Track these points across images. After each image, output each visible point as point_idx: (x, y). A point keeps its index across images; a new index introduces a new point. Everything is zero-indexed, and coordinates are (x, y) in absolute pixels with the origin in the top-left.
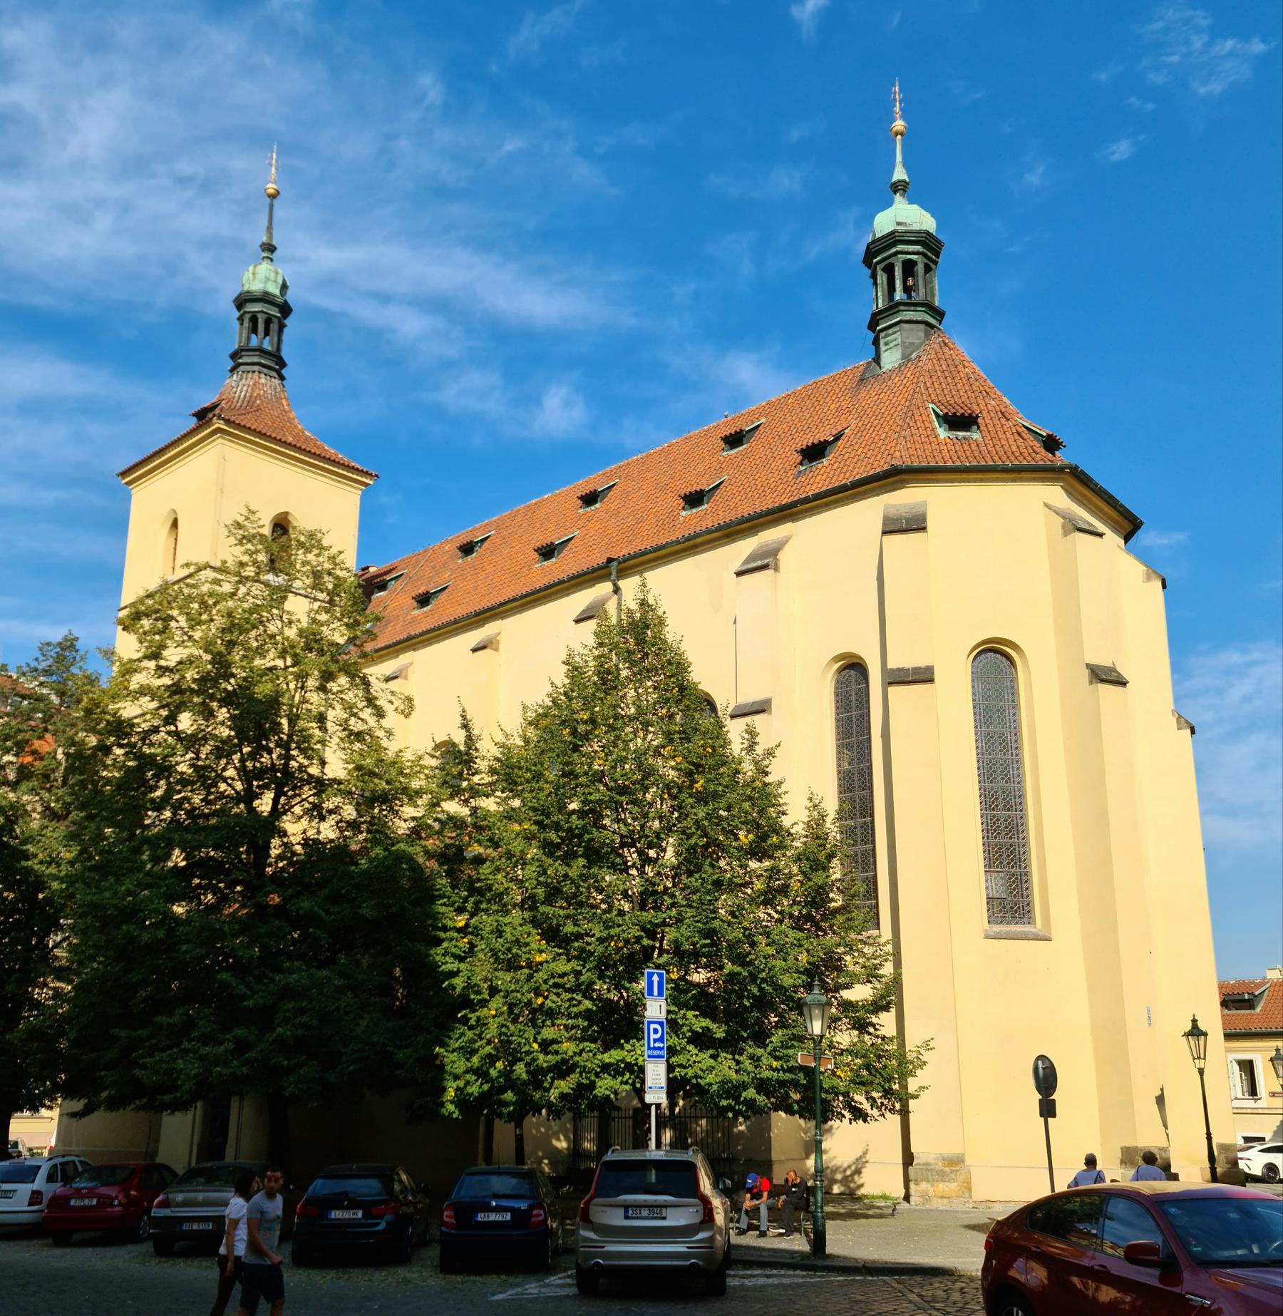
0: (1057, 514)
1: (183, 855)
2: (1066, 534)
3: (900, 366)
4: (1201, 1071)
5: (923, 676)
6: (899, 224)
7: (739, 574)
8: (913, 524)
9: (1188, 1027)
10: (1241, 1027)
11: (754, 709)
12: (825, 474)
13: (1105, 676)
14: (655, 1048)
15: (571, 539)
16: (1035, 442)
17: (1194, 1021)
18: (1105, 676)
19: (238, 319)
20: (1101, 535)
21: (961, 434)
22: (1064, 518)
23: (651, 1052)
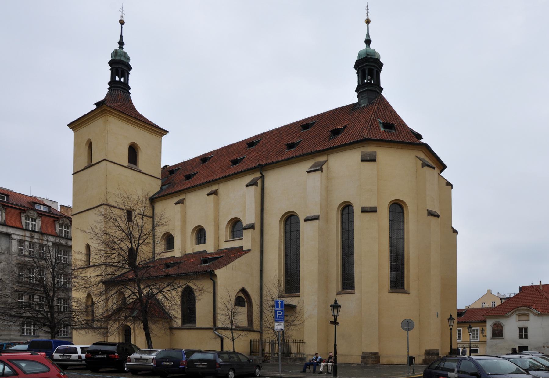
0: (420, 160)
2: (423, 166)
3: (367, 105)
4: (451, 329)
5: (373, 210)
6: (367, 55)
7: (308, 172)
8: (372, 159)
9: (449, 317)
10: (519, 320)
11: (313, 218)
12: (340, 140)
14: (279, 318)
16: (414, 136)
17: (451, 316)
21: (388, 130)
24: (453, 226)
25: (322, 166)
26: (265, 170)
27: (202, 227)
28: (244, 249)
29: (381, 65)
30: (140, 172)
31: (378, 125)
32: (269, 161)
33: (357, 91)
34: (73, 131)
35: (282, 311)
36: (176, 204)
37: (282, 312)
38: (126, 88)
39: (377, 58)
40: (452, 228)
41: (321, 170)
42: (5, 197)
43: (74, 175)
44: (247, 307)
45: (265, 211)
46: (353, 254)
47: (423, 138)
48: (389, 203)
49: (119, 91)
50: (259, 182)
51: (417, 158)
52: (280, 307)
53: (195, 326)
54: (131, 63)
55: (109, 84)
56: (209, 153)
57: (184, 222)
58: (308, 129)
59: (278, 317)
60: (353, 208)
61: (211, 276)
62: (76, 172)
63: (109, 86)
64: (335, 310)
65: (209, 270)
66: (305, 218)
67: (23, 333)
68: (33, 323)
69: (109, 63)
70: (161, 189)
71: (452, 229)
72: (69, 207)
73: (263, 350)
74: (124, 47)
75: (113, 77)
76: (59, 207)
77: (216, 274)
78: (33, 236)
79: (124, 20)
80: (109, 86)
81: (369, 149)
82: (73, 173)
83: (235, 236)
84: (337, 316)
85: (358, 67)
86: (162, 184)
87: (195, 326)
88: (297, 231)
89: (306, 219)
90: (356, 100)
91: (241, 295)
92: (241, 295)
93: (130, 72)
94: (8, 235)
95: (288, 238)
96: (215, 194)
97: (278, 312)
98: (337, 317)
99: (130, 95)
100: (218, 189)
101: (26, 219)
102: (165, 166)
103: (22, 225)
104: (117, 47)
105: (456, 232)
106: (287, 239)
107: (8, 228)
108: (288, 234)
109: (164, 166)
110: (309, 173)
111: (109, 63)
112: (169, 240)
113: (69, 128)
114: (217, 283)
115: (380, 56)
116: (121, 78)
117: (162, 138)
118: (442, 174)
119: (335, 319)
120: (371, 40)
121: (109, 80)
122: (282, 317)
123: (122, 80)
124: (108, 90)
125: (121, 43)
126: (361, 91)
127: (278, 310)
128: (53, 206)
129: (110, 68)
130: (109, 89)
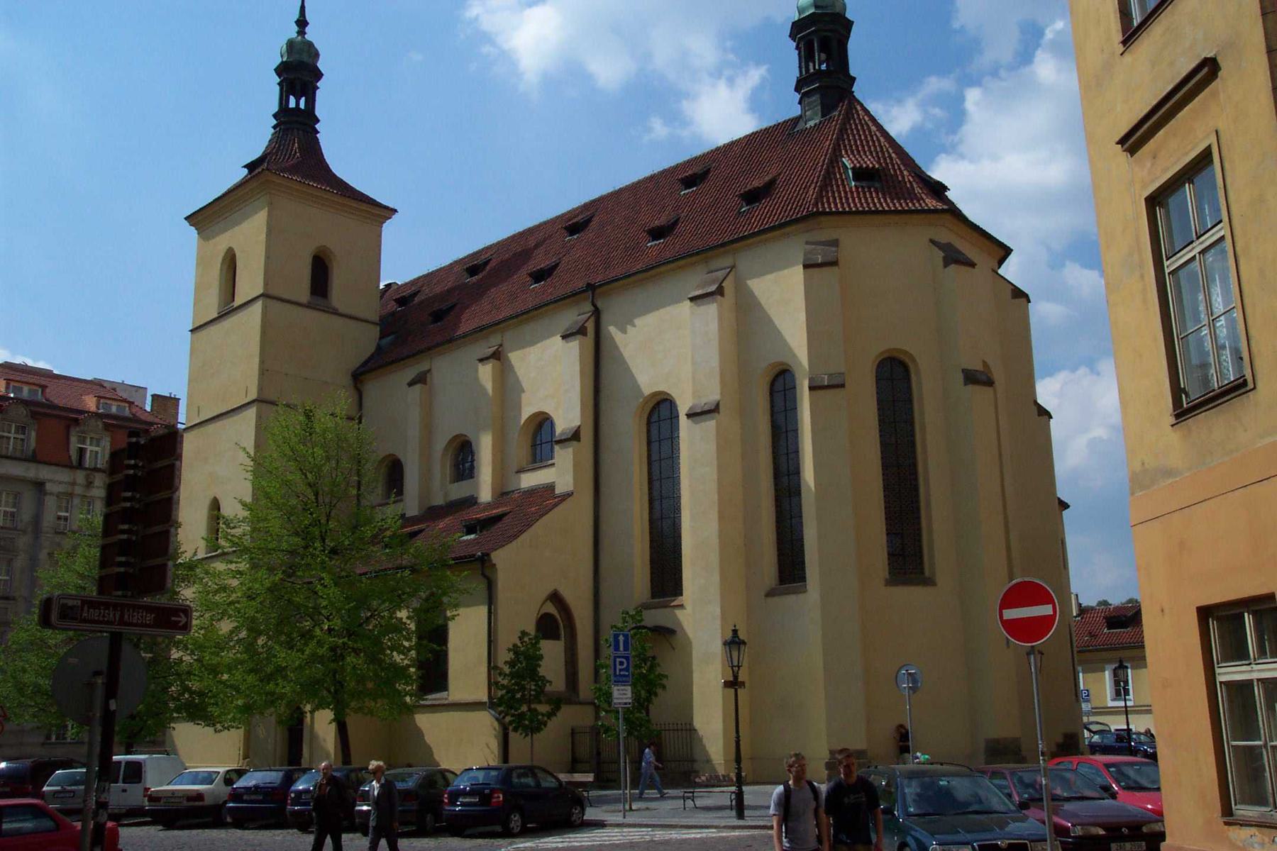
2: (946, 264)
14: (621, 675)
20: (972, 265)
21: (864, 184)
24: (1039, 401)
27: (467, 438)
28: (557, 492)
29: (848, 25)
30: (335, 312)
32: (612, 274)
33: (797, 89)
34: (196, 231)
35: (627, 658)
36: (411, 384)
37: (627, 660)
39: (837, 11)
40: (1036, 403)
42: (38, 391)
44: (563, 639)
45: (603, 395)
47: (949, 187)
48: (882, 353)
49: (295, 130)
51: (933, 247)
52: (621, 648)
53: (446, 699)
54: (321, 65)
55: (275, 116)
57: (428, 429)
58: (694, 187)
59: (618, 673)
61: (482, 564)
62: (198, 325)
63: (275, 122)
64: (733, 652)
65: (479, 554)
66: (689, 411)
67: (48, 737)
69: (275, 70)
70: (379, 348)
72: (170, 397)
73: (599, 754)
74: (307, 29)
75: (283, 101)
76: (149, 399)
77: (494, 562)
78: (91, 483)
80: (275, 122)
82: (191, 328)
83: (538, 458)
84: (739, 667)
85: (799, 36)
86: (381, 333)
87: (446, 699)
88: (673, 438)
89: (690, 412)
90: (796, 111)
91: (551, 609)
92: (551, 609)
93: (318, 84)
94: (39, 486)
95: (655, 457)
97: (618, 660)
98: (739, 669)
99: (318, 135)
101: (79, 442)
102: (388, 286)
103: (70, 457)
104: (292, 32)
106: (653, 459)
107: (41, 466)
108: (655, 446)
111: (275, 70)
113: (188, 224)
114: (497, 584)
116: (300, 99)
117: (382, 227)
118: (1001, 271)
119: (736, 677)
121: (276, 109)
122: (627, 673)
123: (302, 105)
125: (302, 23)
126: (805, 90)
127: (619, 657)
129: (278, 80)
130: (274, 127)
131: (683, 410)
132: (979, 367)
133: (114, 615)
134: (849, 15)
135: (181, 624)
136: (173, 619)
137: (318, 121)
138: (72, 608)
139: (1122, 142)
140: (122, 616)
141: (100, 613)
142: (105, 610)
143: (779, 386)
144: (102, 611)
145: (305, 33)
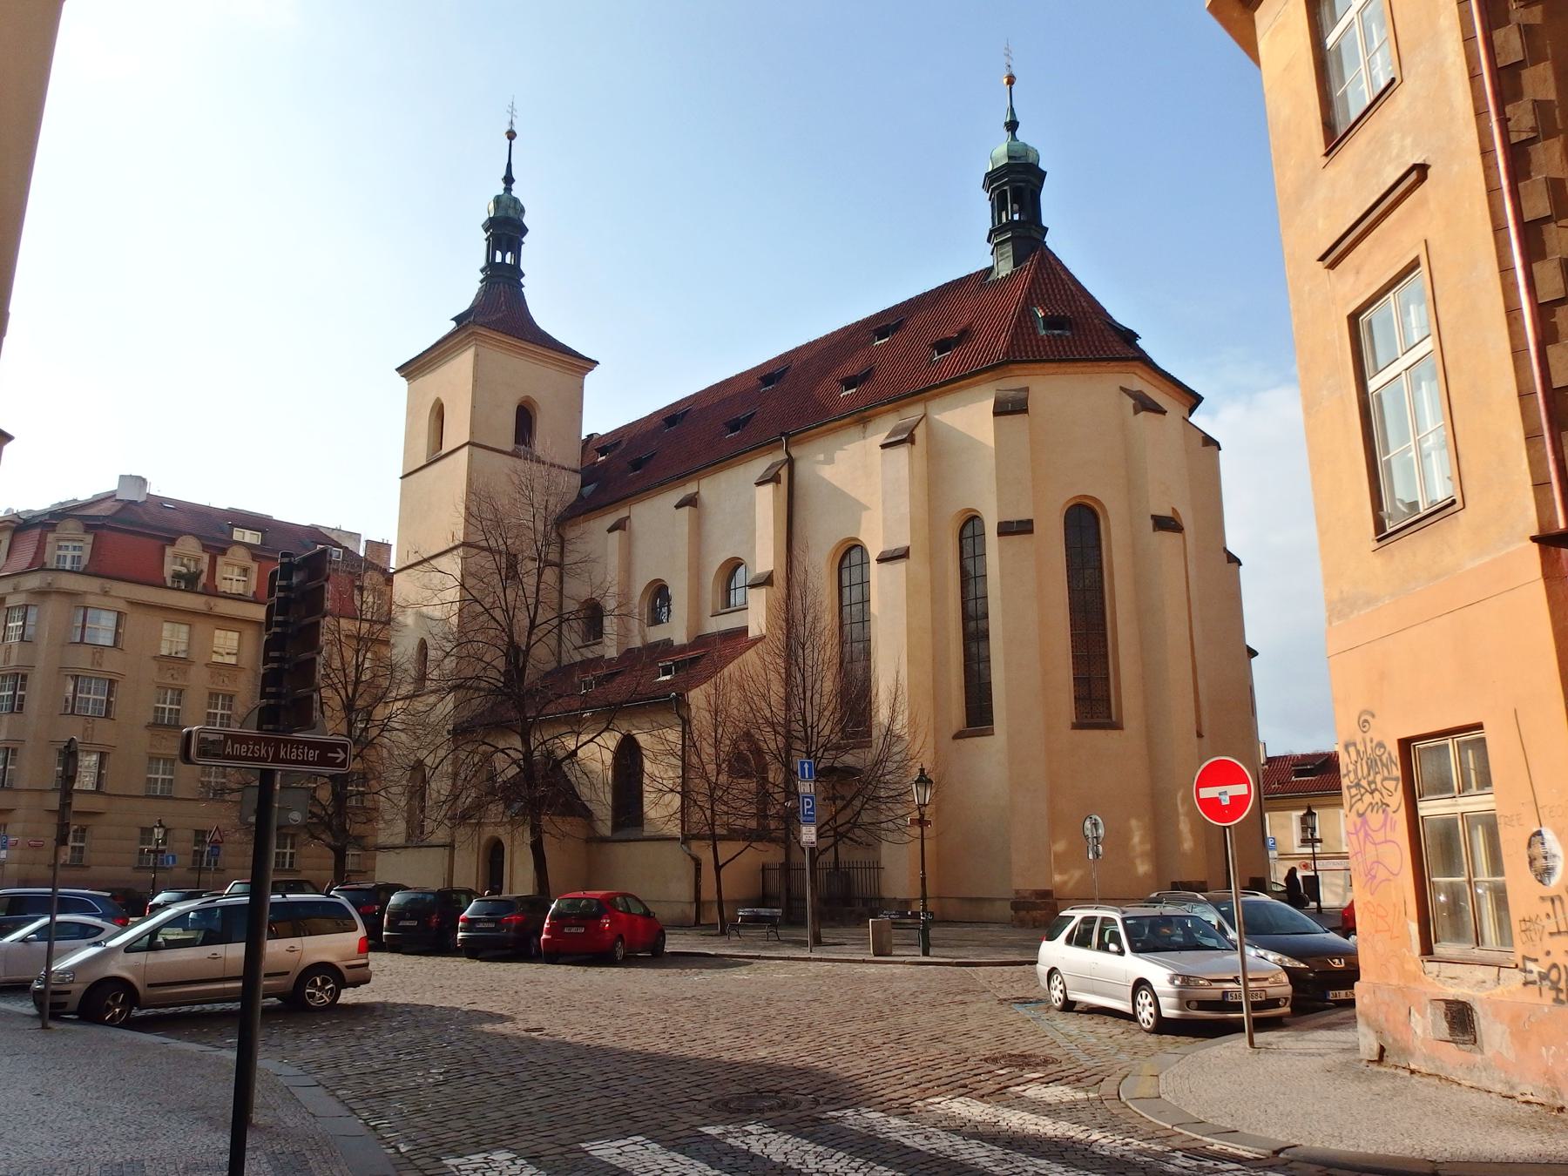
1: (350, 833)
2: (1136, 412)
5: (1023, 528)
7: (884, 446)
13: (1168, 524)
15: (754, 413)
18: (1168, 524)
19: (486, 240)
20: (1164, 412)
22: (1135, 399)
23: (805, 819)
25: (913, 430)
26: (798, 443)
29: (1042, 175)
31: (1032, 323)
38: (515, 272)
39: (1030, 161)
40: (1225, 549)
41: (911, 440)
43: (404, 479)
46: (988, 637)
48: (1074, 498)
50: (784, 473)
54: (526, 220)
56: (682, 400)
60: (983, 522)
68: (1091, 1095)
71: (1225, 555)
74: (514, 186)
76: (363, 545)
79: (515, 129)
81: (1011, 383)
82: (401, 475)
96: (691, 506)
100: (698, 492)
102: (591, 436)
105: (1234, 560)
109: (588, 436)
110: (888, 450)
112: (593, 615)
115: (1038, 155)
118: (1191, 419)
120: (1018, 120)
121: (482, 263)
124: (480, 285)
125: (509, 180)
127: (806, 797)
128: (350, 545)
131: (873, 555)
132: (1169, 513)
133: (267, 752)
134: (1042, 166)
135: (338, 761)
136: (330, 755)
137: (523, 275)
138: (213, 742)
139: (1322, 259)
140: (277, 753)
141: (248, 749)
142: (254, 745)
143: (968, 532)
144: (251, 747)
145: (511, 190)
